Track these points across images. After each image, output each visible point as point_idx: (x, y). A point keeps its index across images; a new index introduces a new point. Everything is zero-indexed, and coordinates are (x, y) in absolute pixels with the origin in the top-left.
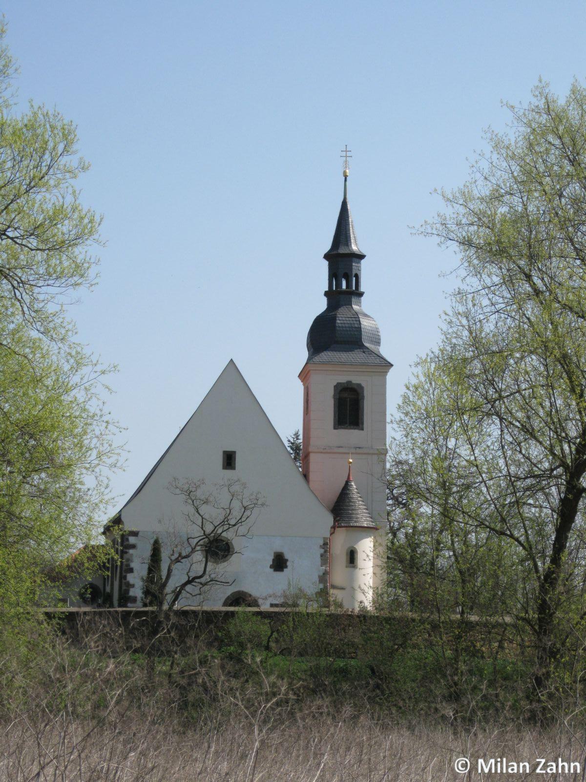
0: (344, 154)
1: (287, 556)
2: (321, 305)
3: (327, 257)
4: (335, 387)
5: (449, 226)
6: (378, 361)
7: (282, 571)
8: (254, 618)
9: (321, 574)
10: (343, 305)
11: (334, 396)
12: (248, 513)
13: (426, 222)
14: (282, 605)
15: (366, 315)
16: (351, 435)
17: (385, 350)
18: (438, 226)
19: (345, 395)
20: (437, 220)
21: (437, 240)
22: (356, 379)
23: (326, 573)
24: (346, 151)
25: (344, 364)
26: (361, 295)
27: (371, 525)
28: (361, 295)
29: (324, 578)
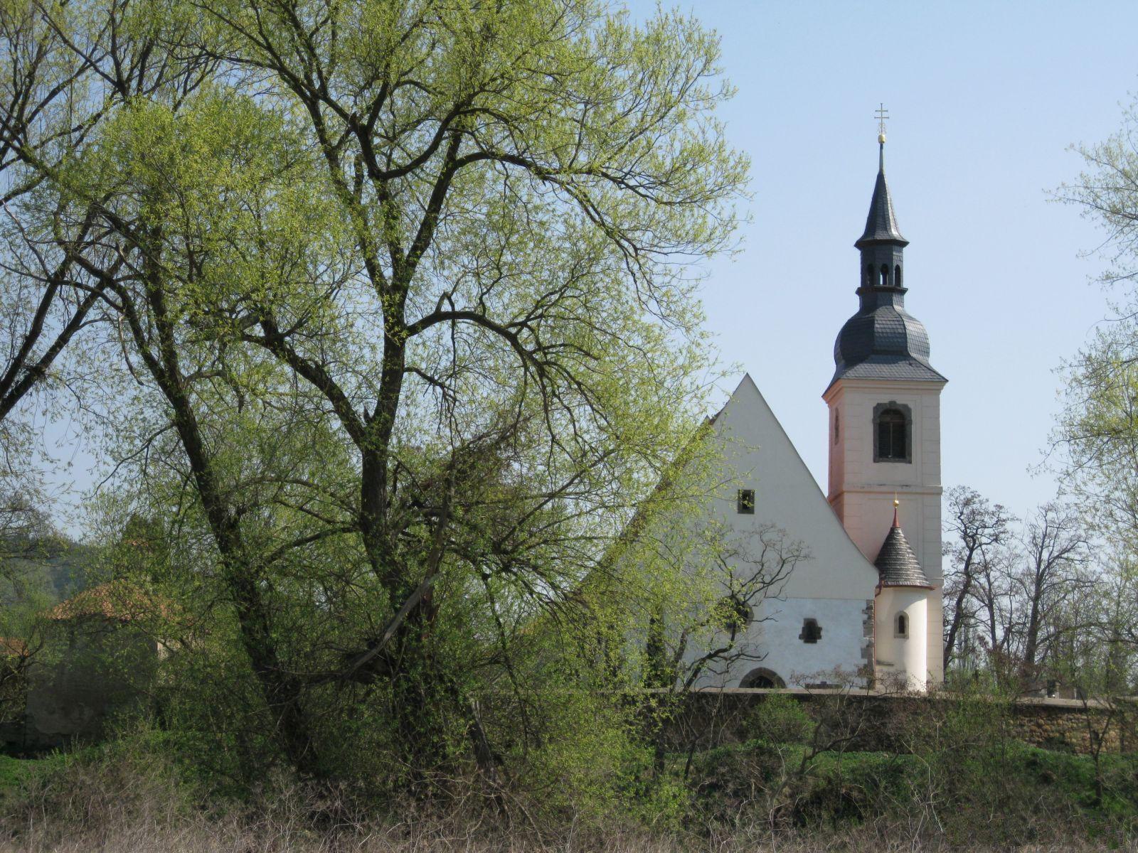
0: (879, 114)
1: (820, 623)
2: (853, 306)
3: (859, 245)
4: (876, 409)
5: (1096, 190)
6: (928, 375)
7: (815, 642)
8: (789, 704)
9: (864, 646)
10: (881, 305)
11: (874, 420)
12: (787, 567)
13: (1063, 184)
14: (819, 686)
15: (911, 318)
16: (894, 470)
17: (936, 361)
18: (1082, 190)
19: (888, 419)
20: (1080, 182)
21: (1081, 208)
22: (901, 399)
23: (870, 645)
24: (882, 111)
25: (887, 380)
26: (903, 292)
27: (925, 583)
28: (903, 292)
29: (867, 651)
